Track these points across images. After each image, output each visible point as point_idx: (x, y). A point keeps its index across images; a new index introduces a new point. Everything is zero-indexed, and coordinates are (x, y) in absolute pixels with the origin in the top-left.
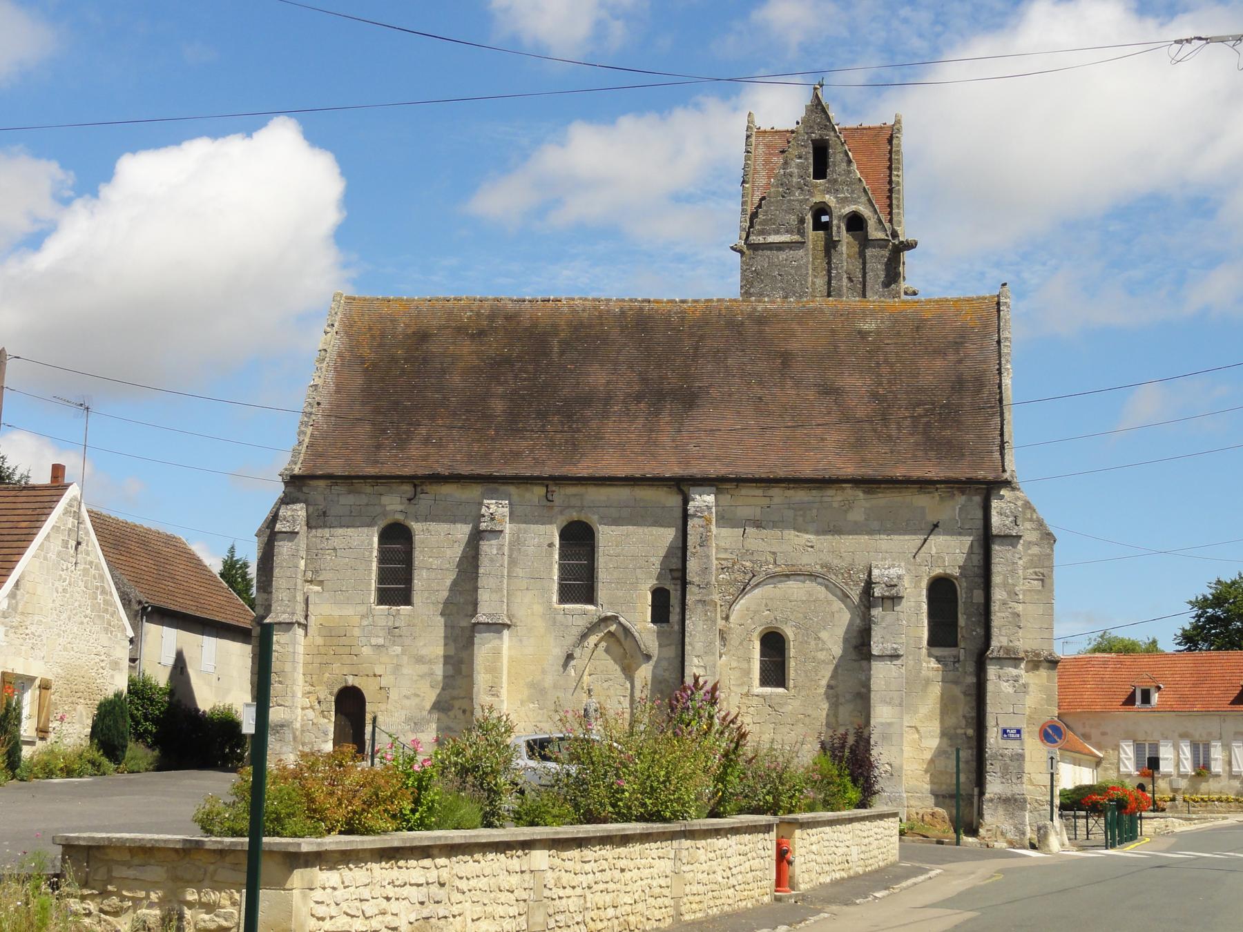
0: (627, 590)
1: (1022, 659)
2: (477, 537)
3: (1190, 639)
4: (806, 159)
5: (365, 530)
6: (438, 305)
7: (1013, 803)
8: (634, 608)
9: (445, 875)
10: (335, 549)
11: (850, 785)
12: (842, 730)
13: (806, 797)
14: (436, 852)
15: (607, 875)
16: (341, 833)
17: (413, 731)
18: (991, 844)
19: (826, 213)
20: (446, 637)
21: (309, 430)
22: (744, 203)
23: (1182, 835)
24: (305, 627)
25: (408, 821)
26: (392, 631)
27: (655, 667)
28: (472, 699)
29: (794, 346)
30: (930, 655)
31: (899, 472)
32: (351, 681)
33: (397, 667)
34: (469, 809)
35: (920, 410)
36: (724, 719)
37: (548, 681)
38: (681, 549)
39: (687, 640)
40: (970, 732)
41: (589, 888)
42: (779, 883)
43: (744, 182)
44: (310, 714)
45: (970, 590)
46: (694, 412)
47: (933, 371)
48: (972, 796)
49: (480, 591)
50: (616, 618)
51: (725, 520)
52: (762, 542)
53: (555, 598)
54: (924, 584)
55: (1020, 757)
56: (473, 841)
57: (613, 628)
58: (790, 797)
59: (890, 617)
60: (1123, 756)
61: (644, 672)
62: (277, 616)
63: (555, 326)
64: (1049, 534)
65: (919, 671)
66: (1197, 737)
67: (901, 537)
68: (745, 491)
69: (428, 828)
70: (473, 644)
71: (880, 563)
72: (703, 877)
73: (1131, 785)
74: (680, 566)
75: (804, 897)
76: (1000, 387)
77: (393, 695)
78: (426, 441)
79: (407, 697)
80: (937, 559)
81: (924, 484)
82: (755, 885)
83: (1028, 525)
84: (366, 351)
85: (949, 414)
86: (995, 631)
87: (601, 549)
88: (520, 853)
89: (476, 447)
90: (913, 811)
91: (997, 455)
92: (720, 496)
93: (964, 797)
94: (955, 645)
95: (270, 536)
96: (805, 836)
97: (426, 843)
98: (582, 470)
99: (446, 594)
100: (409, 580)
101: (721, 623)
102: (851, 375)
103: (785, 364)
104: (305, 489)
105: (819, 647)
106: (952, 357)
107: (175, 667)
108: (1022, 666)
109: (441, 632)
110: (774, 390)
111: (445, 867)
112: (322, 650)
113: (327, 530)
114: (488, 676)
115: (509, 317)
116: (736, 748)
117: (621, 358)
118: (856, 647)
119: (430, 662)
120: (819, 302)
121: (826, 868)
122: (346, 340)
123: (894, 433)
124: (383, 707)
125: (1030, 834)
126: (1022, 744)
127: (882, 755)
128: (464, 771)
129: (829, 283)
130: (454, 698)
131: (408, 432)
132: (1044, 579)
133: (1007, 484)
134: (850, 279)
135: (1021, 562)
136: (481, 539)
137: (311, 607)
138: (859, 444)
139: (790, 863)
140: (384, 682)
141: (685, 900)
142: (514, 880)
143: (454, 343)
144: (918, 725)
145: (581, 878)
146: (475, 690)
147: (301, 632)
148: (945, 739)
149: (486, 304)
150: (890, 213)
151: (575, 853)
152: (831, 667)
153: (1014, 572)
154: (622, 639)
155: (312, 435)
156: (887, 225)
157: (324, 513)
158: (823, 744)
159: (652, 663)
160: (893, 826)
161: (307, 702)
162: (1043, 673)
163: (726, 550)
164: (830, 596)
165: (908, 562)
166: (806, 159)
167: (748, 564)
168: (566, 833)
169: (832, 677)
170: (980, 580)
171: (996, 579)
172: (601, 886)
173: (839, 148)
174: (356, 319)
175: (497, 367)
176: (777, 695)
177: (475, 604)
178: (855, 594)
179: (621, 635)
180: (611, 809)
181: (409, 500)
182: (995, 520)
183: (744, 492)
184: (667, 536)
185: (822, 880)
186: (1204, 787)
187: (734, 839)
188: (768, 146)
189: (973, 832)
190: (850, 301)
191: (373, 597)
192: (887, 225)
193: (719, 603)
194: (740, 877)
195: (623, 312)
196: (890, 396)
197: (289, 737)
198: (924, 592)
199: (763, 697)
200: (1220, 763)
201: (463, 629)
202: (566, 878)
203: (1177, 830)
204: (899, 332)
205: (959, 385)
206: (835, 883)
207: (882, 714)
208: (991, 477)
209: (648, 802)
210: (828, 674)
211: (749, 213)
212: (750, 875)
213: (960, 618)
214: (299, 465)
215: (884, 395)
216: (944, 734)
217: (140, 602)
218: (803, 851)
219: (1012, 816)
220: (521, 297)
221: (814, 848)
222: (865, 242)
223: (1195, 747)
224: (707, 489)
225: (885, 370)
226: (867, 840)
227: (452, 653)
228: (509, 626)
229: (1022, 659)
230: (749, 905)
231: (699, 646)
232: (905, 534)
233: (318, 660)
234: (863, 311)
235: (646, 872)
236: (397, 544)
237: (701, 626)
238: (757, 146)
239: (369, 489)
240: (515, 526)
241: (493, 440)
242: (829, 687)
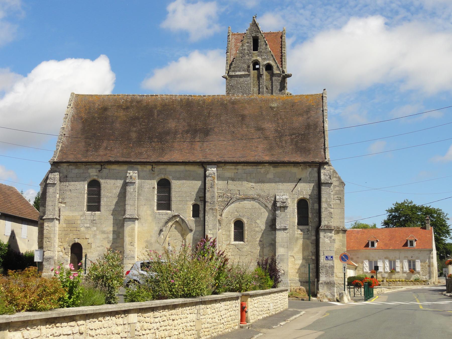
0: (183, 206)
1: (333, 230)
2: (125, 185)
3: (386, 224)
4: (250, 44)
5: (82, 182)
7: (330, 284)
8: (186, 212)
9: (82, 329)
10: (70, 190)
11: (269, 279)
12: (265, 258)
13: (252, 285)
14: (77, 318)
15: (166, 323)
16: (27, 311)
18: (322, 300)
19: (258, 64)
20: (113, 224)
21: (61, 145)
22: (227, 60)
23: (387, 294)
24: (59, 220)
25: (67, 302)
27: (194, 234)
28: (123, 247)
29: (246, 112)
30: (298, 229)
31: (286, 159)
32: (77, 241)
33: (95, 235)
34: (98, 296)
35: (294, 136)
36: (219, 253)
38: (204, 189)
39: (206, 224)
40: (314, 258)
41: (158, 329)
42: (242, 320)
43: (227, 52)
44: (61, 254)
45: (313, 204)
46: (208, 137)
48: (314, 282)
49: (126, 206)
50: (179, 215)
51: (220, 178)
52: (232, 185)
53: (155, 208)
54: (296, 202)
55: (332, 267)
56: (97, 312)
57: (178, 219)
58: (246, 285)
59: (283, 214)
60: (365, 265)
61: (190, 237)
62: (48, 216)
63: (155, 105)
64: (343, 182)
66: (391, 259)
67: (287, 184)
68: (228, 167)
69: (77, 306)
70: (124, 226)
71: (279, 194)
72: (210, 321)
73: (369, 276)
74: (203, 195)
75: (252, 326)
76: (323, 127)
77: (93, 246)
78: (106, 148)
79: (99, 247)
80: (300, 192)
81: (296, 164)
82: (232, 322)
83: (335, 179)
84: (83, 115)
86: (323, 219)
87: (173, 189)
88: (123, 316)
89: (125, 151)
91: (323, 153)
92: (219, 169)
93: (311, 283)
95: (45, 185)
96: (252, 301)
97: (72, 314)
98: (166, 159)
99: (113, 207)
100: (99, 202)
101: (219, 217)
102: (267, 123)
104: (59, 167)
105: (256, 226)
106: (305, 117)
107: (11, 236)
108: (333, 232)
109: (112, 221)
110: (239, 129)
111: (83, 325)
112: (66, 229)
113: (67, 183)
115: (138, 102)
116: (224, 265)
117: (181, 117)
118: (270, 226)
119: (107, 233)
120: (255, 96)
121: (261, 313)
122: (75, 110)
123: (284, 145)
124: (89, 250)
125: (336, 296)
126: (333, 262)
127: (280, 266)
128: (97, 278)
129: (259, 90)
130: (117, 247)
131: (99, 145)
132: (341, 199)
133: (327, 163)
134: (267, 89)
135: (332, 193)
136: (127, 186)
137: (61, 212)
138: (271, 149)
139: (246, 312)
141: (202, 331)
142: (120, 328)
143: (117, 112)
144: (294, 255)
145: (153, 325)
147: (57, 222)
148: (304, 261)
149: (129, 97)
150: (282, 64)
151: (151, 314)
152: (261, 234)
153: (330, 197)
154: (181, 224)
155: (62, 146)
156: (281, 68)
157: (66, 176)
158: (258, 263)
160: (286, 294)
161: (59, 249)
162: (341, 235)
165: (290, 193)
166: (250, 44)
167: (229, 195)
168: (146, 305)
170: (317, 200)
171: (323, 199)
172: (164, 328)
173: (262, 40)
174: (79, 103)
175: (134, 120)
177: (125, 211)
178: (270, 206)
179: (181, 223)
180: (169, 293)
181: (99, 171)
182: (323, 177)
184: (198, 184)
185: (259, 318)
186: (394, 276)
187: (223, 304)
188: (236, 39)
189: (315, 295)
190: (267, 96)
191: (85, 208)
192: (281, 68)
193: (218, 209)
194: (225, 319)
195: (181, 100)
196: (282, 131)
197: (52, 262)
198: (296, 205)
199: (235, 245)
200: (399, 268)
201: (120, 220)
202: (146, 326)
203: (385, 292)
204: (285, 107)
205: (308, 127)
206: (264, 319)
207: (280, 251)
208: (321, 161)
209: (186, 289)
210: (260, 236)
211: (229, 64)
212: (230, 318)
213: (309, 214)
214: (56, 158)
216: (304, 259)
218: (251, 307)
219: (330, 289)
220: (143, 94)
221: (256, 305)
222: (272, 75)
223: (390, 262)
224: (213, 166)
225: (280, 121)
226: (276, 301)
228: (138, 219)
229: (333, 230)
230: (230, 331)
231: (211, 226)
232: (288, 183)
233: (64, 233)
234: (272, 99)
235: (184, 320)
236: (95, 187)
237: (211, 218)
238: (232, 39)
241: (132, 148)
242: (260, 241)
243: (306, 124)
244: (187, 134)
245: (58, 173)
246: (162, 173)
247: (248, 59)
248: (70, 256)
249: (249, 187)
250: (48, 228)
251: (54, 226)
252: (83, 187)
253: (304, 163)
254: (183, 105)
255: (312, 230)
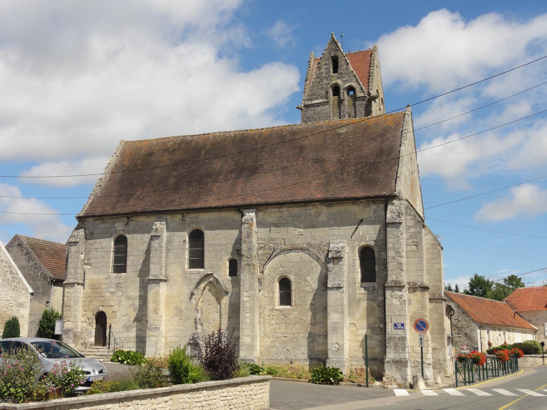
4: (329, 65)
5: (108, 239)
6: (160, 141)
17: (126, 331)
18: (386, 386)
20: (140, 287)
24: (83, 285)
26: (118, 286)
27: (230, 298)
30: (361, 286)
31: (342, 196)
32: (101, 309)
33: (120, 302)
35: (360, 166)
37: (183, 306)
44: (85, 325)
47: (369, 148)
49: (151, 265)
52: (277, 233)
53: (187, 266)
54: (357, 250)
55: (404, 339)
57: (211, 279)
59: (337, 267)
61: (226, 300)
65: (355, 295)
67: (345, 227)
71: (334, 241)
77: (118, 315)
79: (124, 316)
81: (355, 200)
85: (373, 167)
90: (354, 367)
91: (393, 184)
92: (259, 214)
94: (375, 281)
99: (140, 267)
103: (301, 151)
104: (85, 223)
112: (90, 295)
114: (154, 305)
119: (133, 299)
124: (114, 320)
126: (405, 332)
133: (394, 197)
138: (327, 184)
140: (114, 309)
143: (162, 156)
144: (355, 322)
146: (148, 311)
148: (369, 330)
152: (312, 295)
154: (216, 285)
159: (229, 295)
162: (418, 293)
163: (261, 239)
164: (311, 259)
165: (347, 241)
166: (329, 65)
169: (313, 300)
173: (343, 59)
175: (176, 164)
176: (287, 309)
179: (215, 283)
182: (389, 215)
183: (270, 210)
191: (111, 269)
195: (235, 136)
198: (357, 255)
199: (280, 310)
215: (343, 161)
216: (369, 327)
217: (50, 278)
219: (400, 370)
222: (355, 98)
224: (252, 210)
227: (142, 294)
228: (166, 281)
231: (247, 286)
237: (248, 276)
238: (313, 65)
239: (110, 221)
240: (169, 233)
241: (165, 195)
242: (312, 304)
243: (378, 150)
244: (232, 174)
245: (83, 230)
246: (194, 223)
247: (326, 84)
248: (95, 327)
249: (295, 235)
250: (68, 294)
251: (76, 292)
252: (110, 243)
253: (365, 198)
254: (235, 142)
255: (378, 288)
